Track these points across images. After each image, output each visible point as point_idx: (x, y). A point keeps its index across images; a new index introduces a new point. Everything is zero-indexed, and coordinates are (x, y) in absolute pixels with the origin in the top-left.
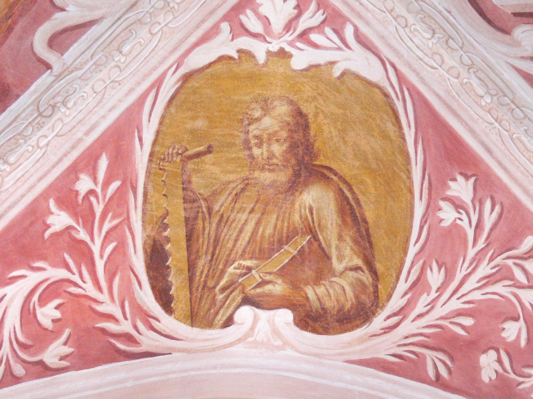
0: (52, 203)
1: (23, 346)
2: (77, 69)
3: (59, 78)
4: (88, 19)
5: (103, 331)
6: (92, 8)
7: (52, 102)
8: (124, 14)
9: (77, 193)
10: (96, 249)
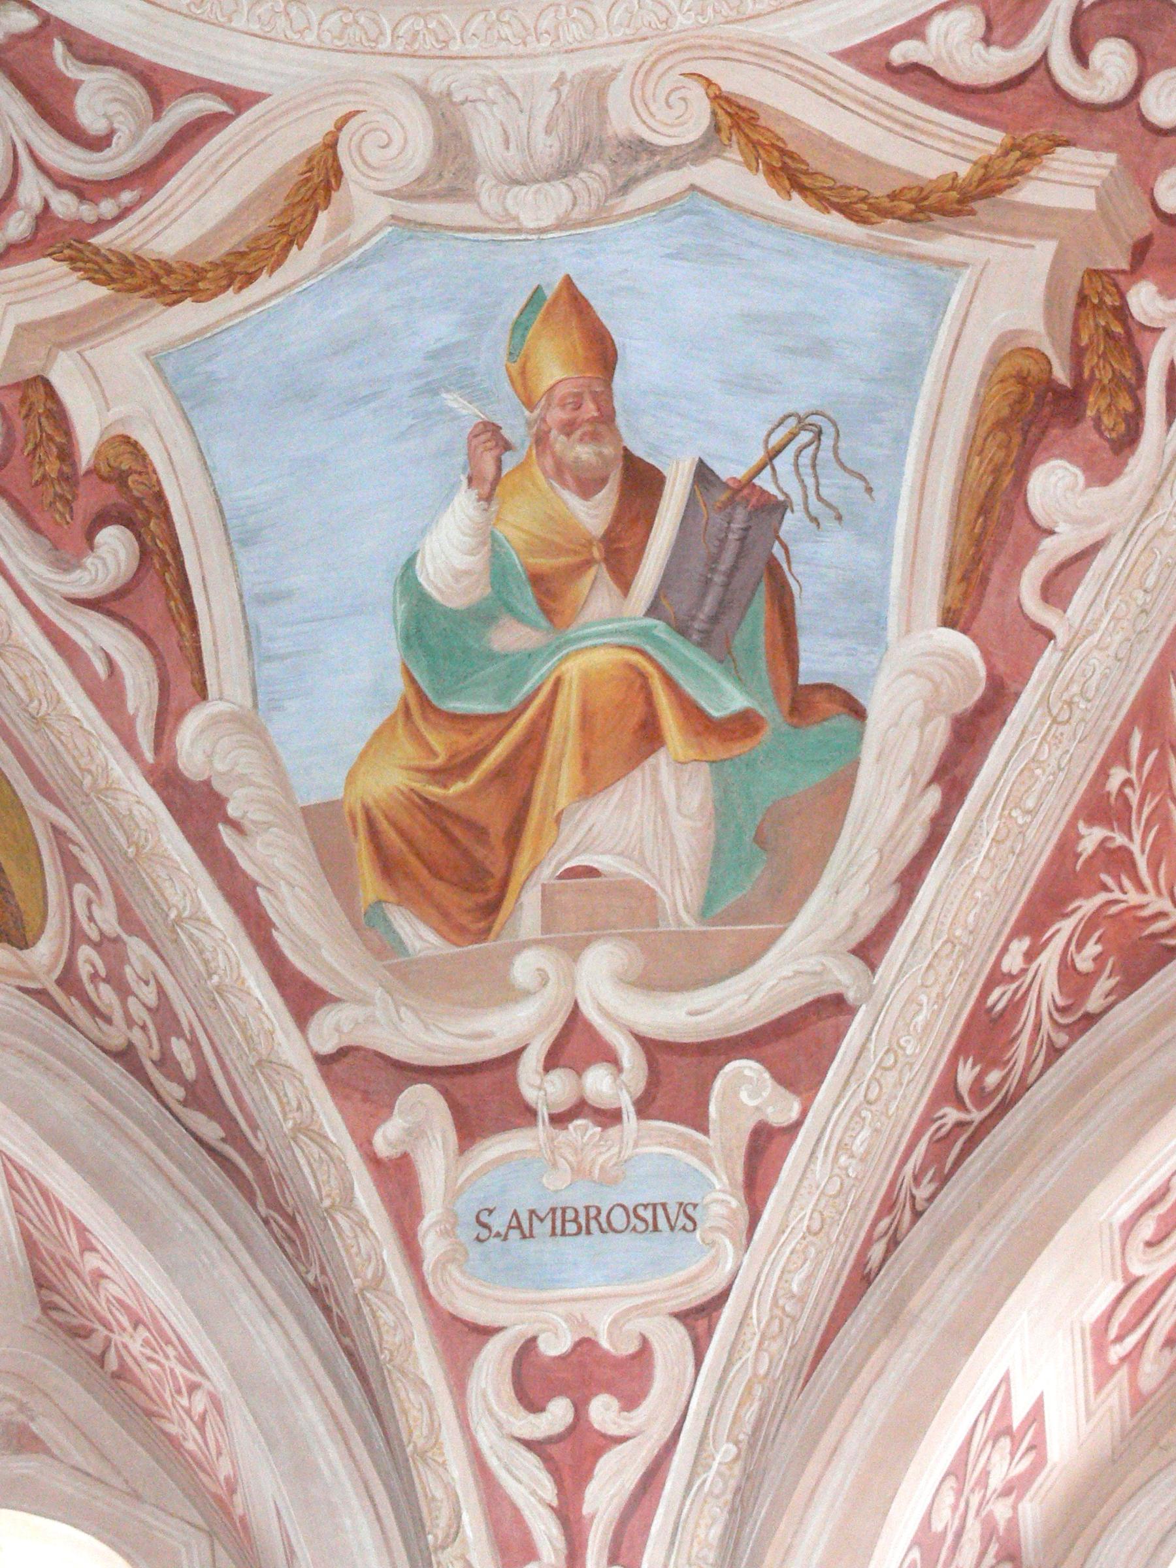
0: (1081, 826)
1: (1063, 1010)
2: (1090, 633)
3: (1067, 652)
4: (1089, 541)
5: (1154, 936)
6: (1090, 522)
7: (1066, 697)
8: (1138, 524)
9: (1109, 794)
10: (1135, 848)
